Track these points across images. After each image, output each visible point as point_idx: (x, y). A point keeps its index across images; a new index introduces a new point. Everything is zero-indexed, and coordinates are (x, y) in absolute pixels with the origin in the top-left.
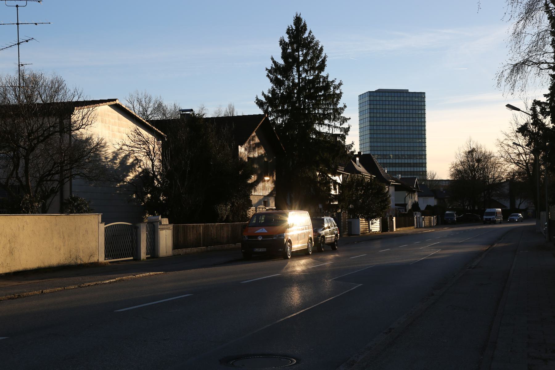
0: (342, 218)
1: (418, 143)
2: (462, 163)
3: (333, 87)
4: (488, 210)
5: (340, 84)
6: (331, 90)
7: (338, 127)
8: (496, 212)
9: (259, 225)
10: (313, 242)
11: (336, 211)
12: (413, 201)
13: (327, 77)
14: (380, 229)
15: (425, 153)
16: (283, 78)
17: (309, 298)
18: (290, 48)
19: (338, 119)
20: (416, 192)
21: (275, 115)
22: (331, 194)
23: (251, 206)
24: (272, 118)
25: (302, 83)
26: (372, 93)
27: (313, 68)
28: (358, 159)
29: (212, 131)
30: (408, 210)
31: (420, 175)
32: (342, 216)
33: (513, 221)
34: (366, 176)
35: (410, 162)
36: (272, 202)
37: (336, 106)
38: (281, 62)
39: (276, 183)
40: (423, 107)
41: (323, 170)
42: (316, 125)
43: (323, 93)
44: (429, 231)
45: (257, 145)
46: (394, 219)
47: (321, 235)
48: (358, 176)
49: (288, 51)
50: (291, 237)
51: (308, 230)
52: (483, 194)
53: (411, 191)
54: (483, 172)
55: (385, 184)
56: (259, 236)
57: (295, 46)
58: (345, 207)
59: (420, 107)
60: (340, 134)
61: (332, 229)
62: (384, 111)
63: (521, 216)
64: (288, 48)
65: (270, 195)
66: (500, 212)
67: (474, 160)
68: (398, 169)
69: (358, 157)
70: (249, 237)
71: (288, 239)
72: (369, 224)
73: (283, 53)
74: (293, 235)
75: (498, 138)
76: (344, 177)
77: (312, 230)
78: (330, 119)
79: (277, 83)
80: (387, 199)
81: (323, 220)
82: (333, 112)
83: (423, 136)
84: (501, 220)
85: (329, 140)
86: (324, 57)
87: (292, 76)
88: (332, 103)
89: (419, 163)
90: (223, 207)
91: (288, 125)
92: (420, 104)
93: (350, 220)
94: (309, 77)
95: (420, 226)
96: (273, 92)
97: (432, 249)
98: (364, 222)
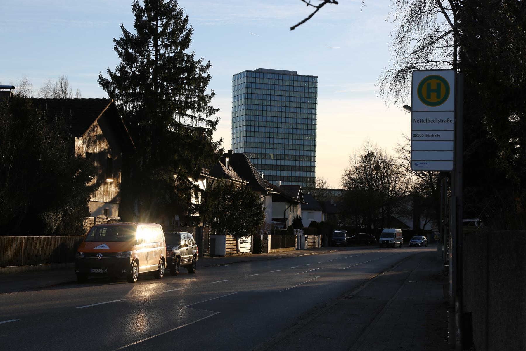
0: (203, 234)
1: (306, 141)
2: (358, 170)
3: (199, 68)
4: (386, 230)
5: (208, 66)
6: (197, 73)
7: (203, 119)
8: (396, 233)
9: (99, 240)
10: (166, 263)
11: (196, 225)
12: (295, 215)
13: (193, 55)
14: (251, 249)
15: (315, 154)
16: (135, 53)
17: (158, 325)
18: (146, 15)
19: (204, 109)
20: (299, 204)
21: (123, 100)
22: (192, 203)
23: (89, 215)
24: (119, 103)
25: (159, 60)
26: (251, 73)
27: (175, 43)
28: (227, 159)
29: (43, 119)
30: (287, 227)
31: (306, 182)
32: (204, 231)
33: (415, 245)
34: (237, 182)
35: (294, 165)
36: (115, 211)
37: (201, 93)
38: (134, 32)
39: (121, 186)
40: (314, 95)
41: (183, 173)
42: (176, 115)
43: (186, 75)
44: (312, 254)
45: (99, 138)
46: (270, 236)
47: (176, 255)
48: (226, 181)
49: (143, 19)
50: (139, 255)
51: (160, 248)
52: (381, 210)
53: (293, 203)
54: (382, 182)
55: (259, 193)
56: (98, 253)
57: (152, 13)
58: (208, 220)
59: (310, 96)
60: (205, 129)
61: (189, 247)
62: (265, 97)
63: (425, 240)
64: (144, 16)
65: (113, 201)
66: (399, 233)
67: (372, 167)
68: (279, 173)
69: (228, 157)
70: (86, 254)
71: (134, 258)
72: (237, 243)
73: (136, 20)
74: (141, 253)
75: (398, 142)
76: (209, 182)
77: (165, 248)
78: (193, 109)
79: (127, 58)
80: (261, 212)
81: (179, 235)
82: (199, 100)
83: (313, 132)
84: (401, 243)
85: (191, 134)
86: (189, 29)
87: (147, 51)
88: (197, 88)
89: (307, 167)
90: (53, 215)
91: (140, 114)
92: (311, 91)
93: (213, 237)
94: (169, 54)
95: (301, 247)
96: (122, 69)
97: (309, 276)
98: (231, 239)
